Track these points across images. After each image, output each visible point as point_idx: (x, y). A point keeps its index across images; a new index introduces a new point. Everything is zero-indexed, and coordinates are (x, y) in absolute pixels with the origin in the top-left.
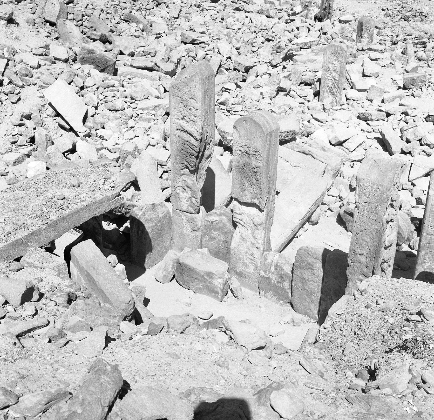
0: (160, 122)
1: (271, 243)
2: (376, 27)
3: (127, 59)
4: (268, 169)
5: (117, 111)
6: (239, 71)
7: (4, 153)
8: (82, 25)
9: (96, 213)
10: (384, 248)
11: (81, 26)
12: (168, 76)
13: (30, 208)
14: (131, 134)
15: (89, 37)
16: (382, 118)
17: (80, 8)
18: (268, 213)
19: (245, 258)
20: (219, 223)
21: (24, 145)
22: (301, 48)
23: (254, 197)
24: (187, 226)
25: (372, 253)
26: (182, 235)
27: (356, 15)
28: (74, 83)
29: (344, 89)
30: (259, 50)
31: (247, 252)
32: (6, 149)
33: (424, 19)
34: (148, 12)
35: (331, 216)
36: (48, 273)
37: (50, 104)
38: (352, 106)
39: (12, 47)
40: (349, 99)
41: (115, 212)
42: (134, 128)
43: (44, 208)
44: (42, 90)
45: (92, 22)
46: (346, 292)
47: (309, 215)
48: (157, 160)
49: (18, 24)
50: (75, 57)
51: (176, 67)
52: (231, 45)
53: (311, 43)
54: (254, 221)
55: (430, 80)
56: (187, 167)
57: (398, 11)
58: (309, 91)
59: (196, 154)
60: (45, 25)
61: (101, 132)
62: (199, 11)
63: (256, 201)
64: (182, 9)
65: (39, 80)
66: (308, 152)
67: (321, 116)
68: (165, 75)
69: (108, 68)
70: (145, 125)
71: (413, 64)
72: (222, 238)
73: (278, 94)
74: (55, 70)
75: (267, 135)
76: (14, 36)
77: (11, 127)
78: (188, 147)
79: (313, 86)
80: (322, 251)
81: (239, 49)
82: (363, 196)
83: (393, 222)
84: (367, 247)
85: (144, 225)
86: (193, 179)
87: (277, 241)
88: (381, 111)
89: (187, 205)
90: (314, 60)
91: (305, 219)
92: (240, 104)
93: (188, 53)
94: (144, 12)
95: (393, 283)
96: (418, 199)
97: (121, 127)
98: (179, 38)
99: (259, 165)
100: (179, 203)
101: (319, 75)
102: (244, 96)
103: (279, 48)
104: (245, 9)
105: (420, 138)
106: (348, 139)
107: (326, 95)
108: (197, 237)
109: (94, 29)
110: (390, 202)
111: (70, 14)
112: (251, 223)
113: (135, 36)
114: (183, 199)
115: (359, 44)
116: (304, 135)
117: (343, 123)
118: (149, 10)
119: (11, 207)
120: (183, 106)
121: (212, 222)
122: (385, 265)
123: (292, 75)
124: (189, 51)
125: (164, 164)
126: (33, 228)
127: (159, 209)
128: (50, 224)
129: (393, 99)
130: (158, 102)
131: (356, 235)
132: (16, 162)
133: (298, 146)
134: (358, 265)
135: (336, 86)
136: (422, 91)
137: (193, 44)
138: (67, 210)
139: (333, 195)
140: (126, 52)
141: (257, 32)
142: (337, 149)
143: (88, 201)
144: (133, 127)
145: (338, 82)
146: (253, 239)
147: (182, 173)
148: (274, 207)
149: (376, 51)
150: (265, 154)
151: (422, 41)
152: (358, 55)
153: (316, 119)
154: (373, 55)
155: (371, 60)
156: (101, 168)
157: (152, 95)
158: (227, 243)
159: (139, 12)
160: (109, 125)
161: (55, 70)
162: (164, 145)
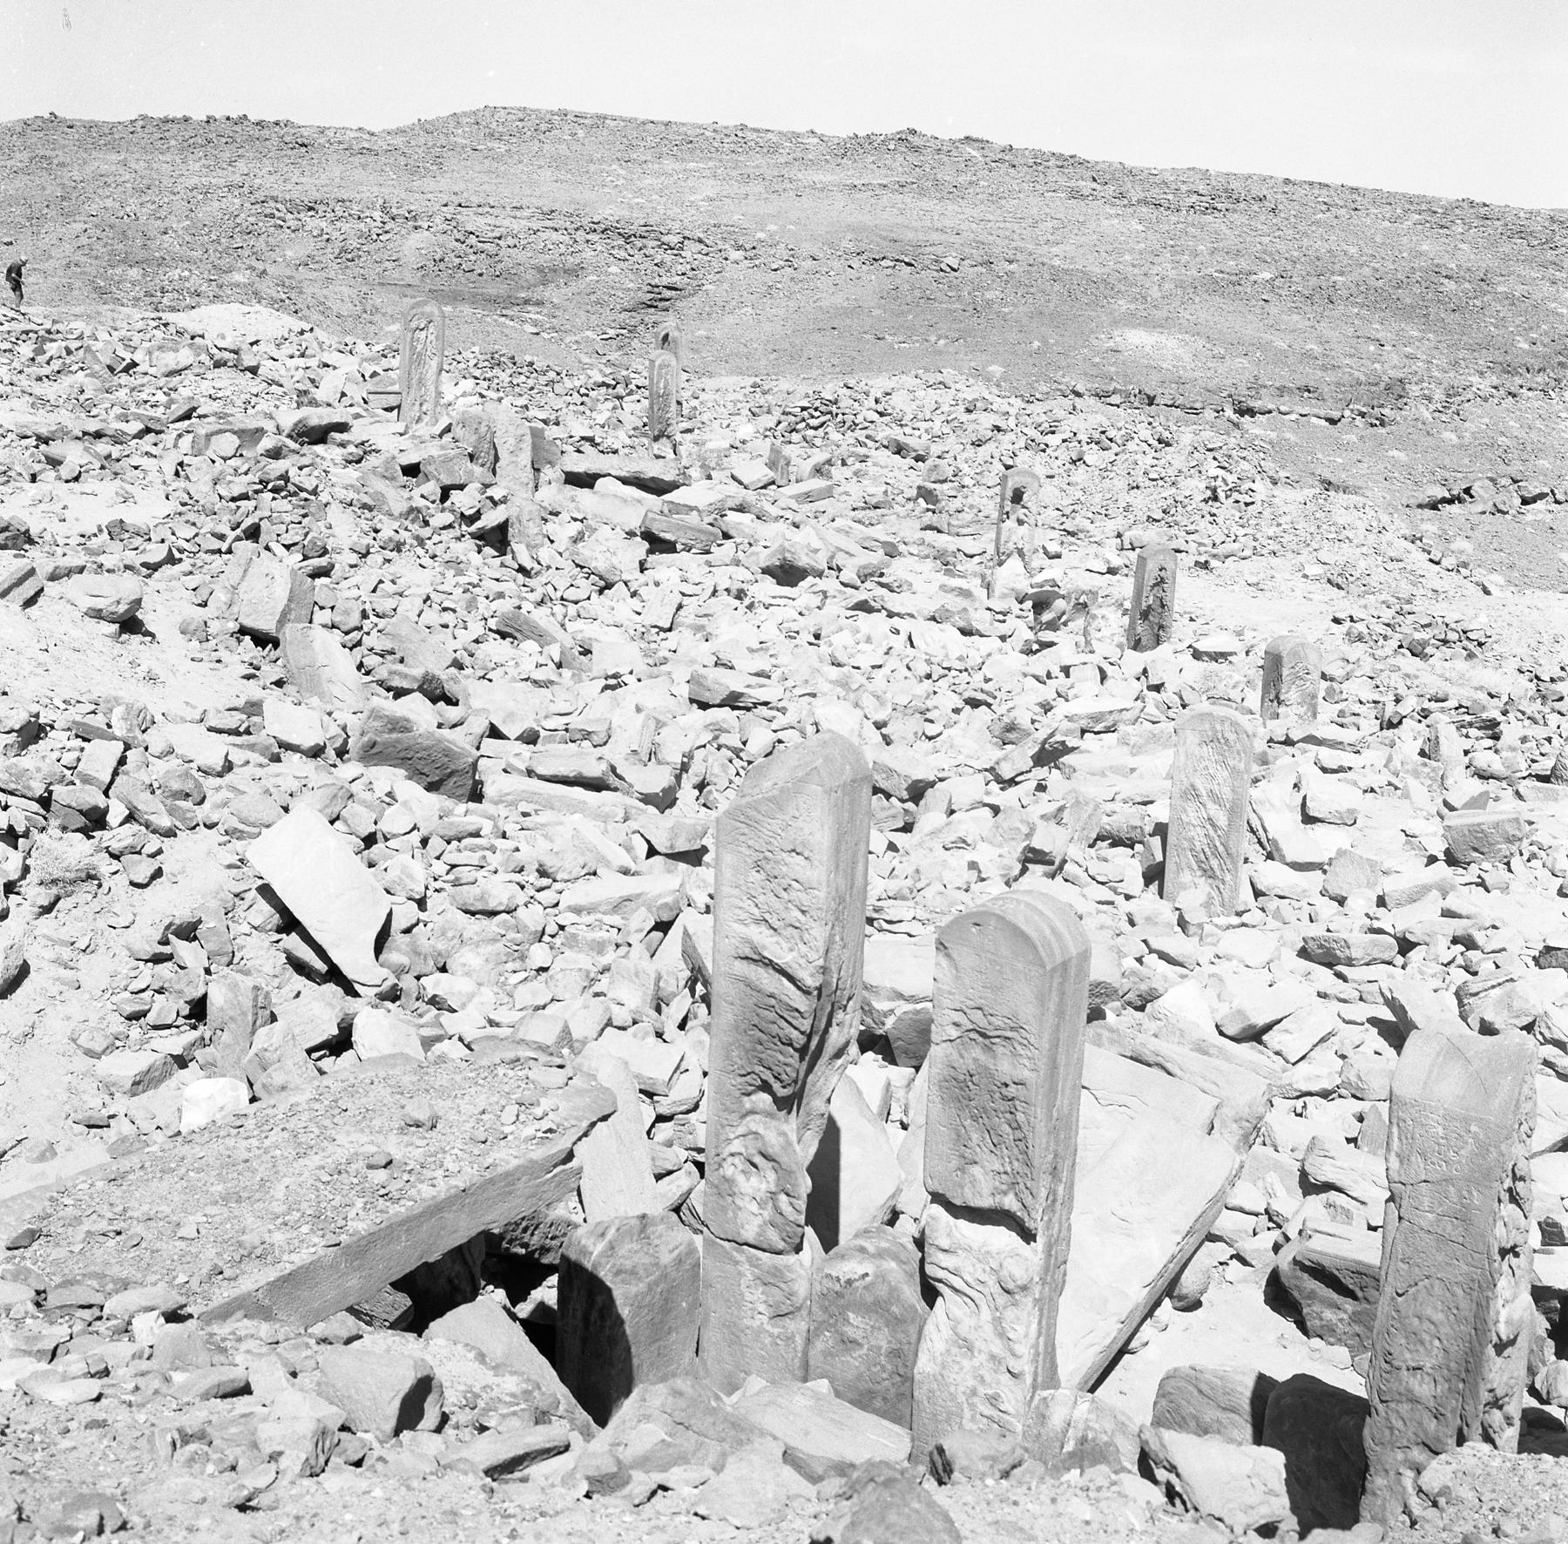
0: (638, 951)
1: (1059, 1360)
2: (1324, 676)
3: (513, 752)
4: (1053, 1090)
5: (492, 914)
6: (888, 796)
7: (99, 1049)
8: (359, 643)
9: (489, 1218)
10: (1495, 1346)
11: (355, 646)
12: (651, 809)
13: (279, 1191)
14: (537, 991)
15: (381, 683)
16: (1386, 957)
17: (355, 593)
18: (1049, 1247)
19: (967, 1414)
20: (872, 1283)
21: (169, 1027)
22: (1083, 732)
23: (1004, 1187)
24: (756, 1297)
25: (1453, 1365)
26: (735, 1335)
27: (1248, 635)
28: (345, 822)
29: (1246, 861)
30: (946, 733)
31: (974, 1392)
32: (107, 1037)
33: (1477, 651)
34: (572, 609)
35: (1244, 1280)
36: (445, 1352)
37: (266, 891)
38: (1277, 915)
39: (140, 705)
40: (1264, 895)
41: (510, 1242)
42: (550, 972)
43: (325, 1192)
44: (238, 845)
45: (393, 636)
46: (1365, 1513)
47: (1169, 1276)
48: (637, 1076)
49: (153, 635)
50: (346, 742)
51: (678, 778)
52: (859, 713)
53: (1116, 716)
54: (1004, 1273)
55: (1534, 838)
56: (765, 1087)
57: (1388, 625)
58: (1127, 866)
59: (802, 1040)
60: (239, 641)
61: (437, 984)
62: (742, 609)
63: (1010, 1203)
64: (686, 601)
65: (226, 810)
66: (1151, 1059)
67: (1175, 944)
68: (641, 805)
69: (453, 778)
70: (584, 961)
71: (1465, 787)
72: (883, 1340)
73: (1024, 871)
74: (279, 781)
75: (1054, 970)
76: (141, 671)
77: (125, 966)
78: (772, 1016)
79: (1138, 847)
80: (1250, 1383)
81: (885, 724)
82: (1417, 1160)
83: (1517, 1255)
84: (1437, 1343)
85: (608, 1291)
86: (785, 1127)
87: (1076, 1361)
88: (1380, 931)
89: (759, 1221)
90: (1133, 770)
91: (1162, 1284)
92: (904, 898)
93: (716, 738)
94: (559, 609)
95: (1543, 1466)
96: (1548, 1224)
97: (501, 968)
98: (684, 691)
99: (1026, 1074)
100: (730, 1214)
101: (1160, 812)
102: (918, 871)
103: (1011, 728)
104: (889, 606)
105: (1530, 1019)
106: (1279, 1021)
107: (1186, 877)
108: (790, 1339)
109: (398, 656)
110: (1508, 1183)
111: (322, 608)
112: (991, 1283)
113: (535, 682)
114: (747, 1199)
115: (1271, 724)
116: (1129, 1004)
117: (1252, 969)
118: (576, 603)
119: (212, 1189)
120: (763, 876)
121: (849, 1282)
122: (1496, 1417)
123: (1066, 812)
124: (718, 730)
125: (661, 1089)
126: (293, 1257)
127: (660, 1236)
128: (348, 1246)
129: (1414, 897)
130: (629, 886)
131: (1393, 1299)
132: (141, 1084)
133: (1115, 1036)
134: (1405, 1408)
135: (1221, 849)
136: (1510, 870)
137: (734, 708)
138: (402, 1202)
139: (1247, 1207)
140: (512, 730)
141: (935, 677)
142: (1246, 1050)
143: (468, 1175)
144: (545, 970)
145: (1227, 834)
146: (998, 1341)
147: (748, 1106)
148: (1069, 1229)
149: (1335, 745)
150: (1046, 1036)
151: (1484, 716)
152: (1276, 758)
153: (1163, 956)
154: (1330, 757)
155: (1324, 770)
156: (501, 1071)
157: (608, 864)
158: (903, 1357)
159: (544, 610)
160: (463, 960)
161: (279, 781)
162: (658, 1025)
